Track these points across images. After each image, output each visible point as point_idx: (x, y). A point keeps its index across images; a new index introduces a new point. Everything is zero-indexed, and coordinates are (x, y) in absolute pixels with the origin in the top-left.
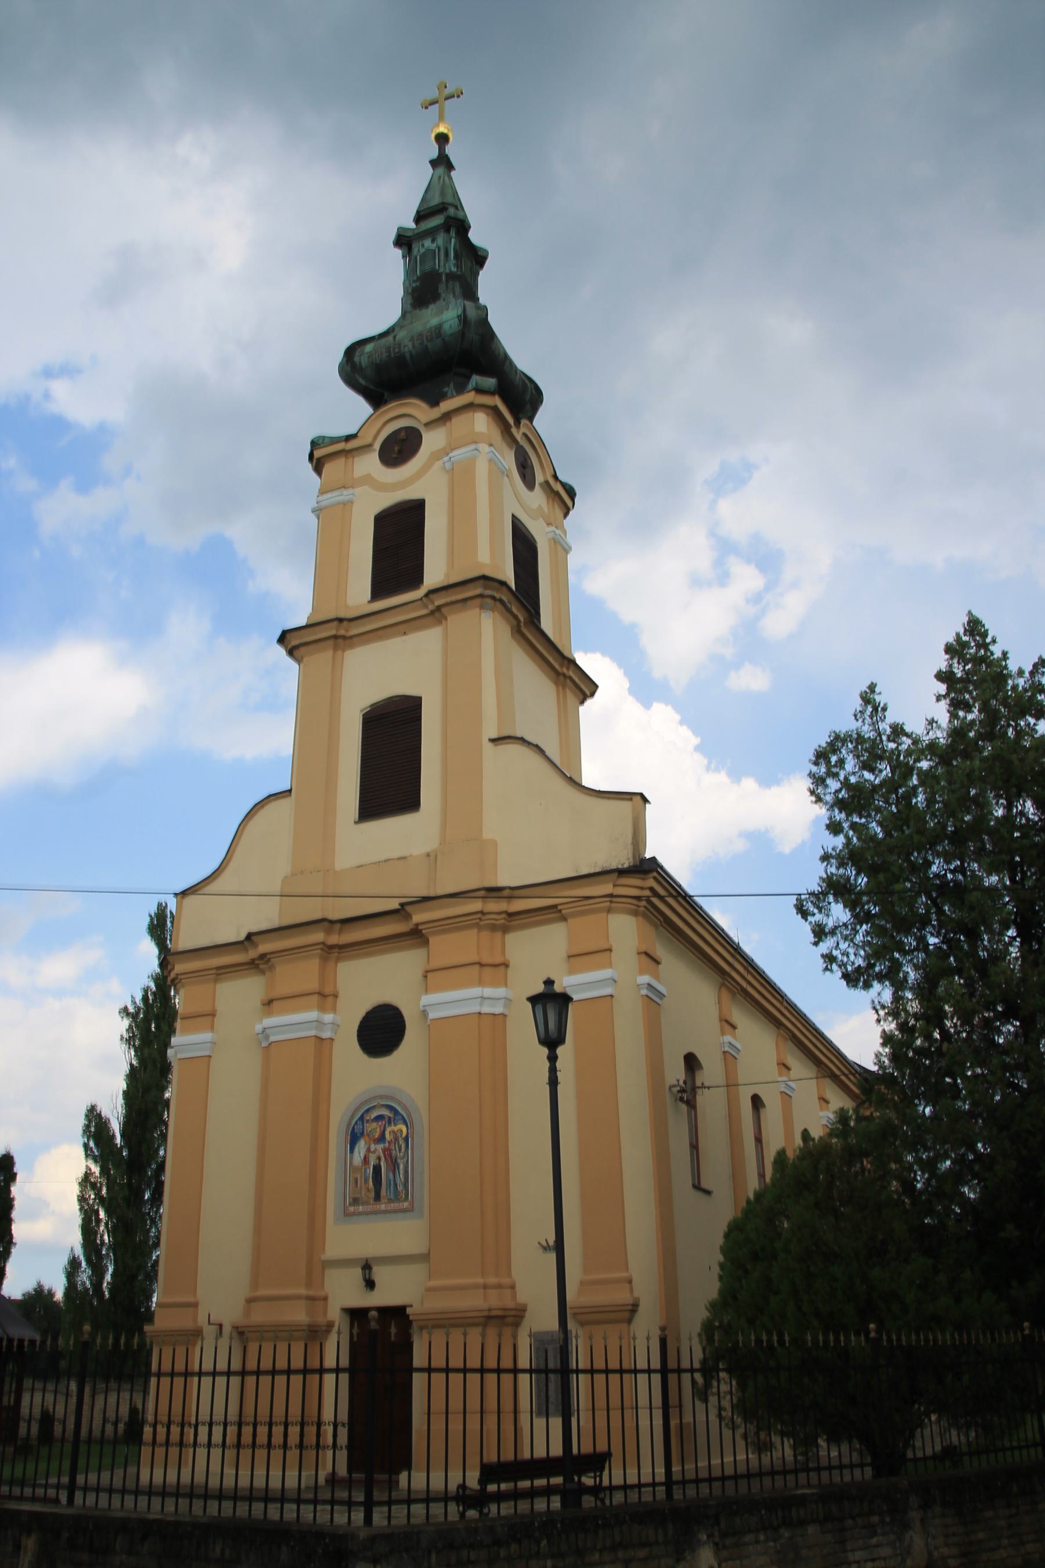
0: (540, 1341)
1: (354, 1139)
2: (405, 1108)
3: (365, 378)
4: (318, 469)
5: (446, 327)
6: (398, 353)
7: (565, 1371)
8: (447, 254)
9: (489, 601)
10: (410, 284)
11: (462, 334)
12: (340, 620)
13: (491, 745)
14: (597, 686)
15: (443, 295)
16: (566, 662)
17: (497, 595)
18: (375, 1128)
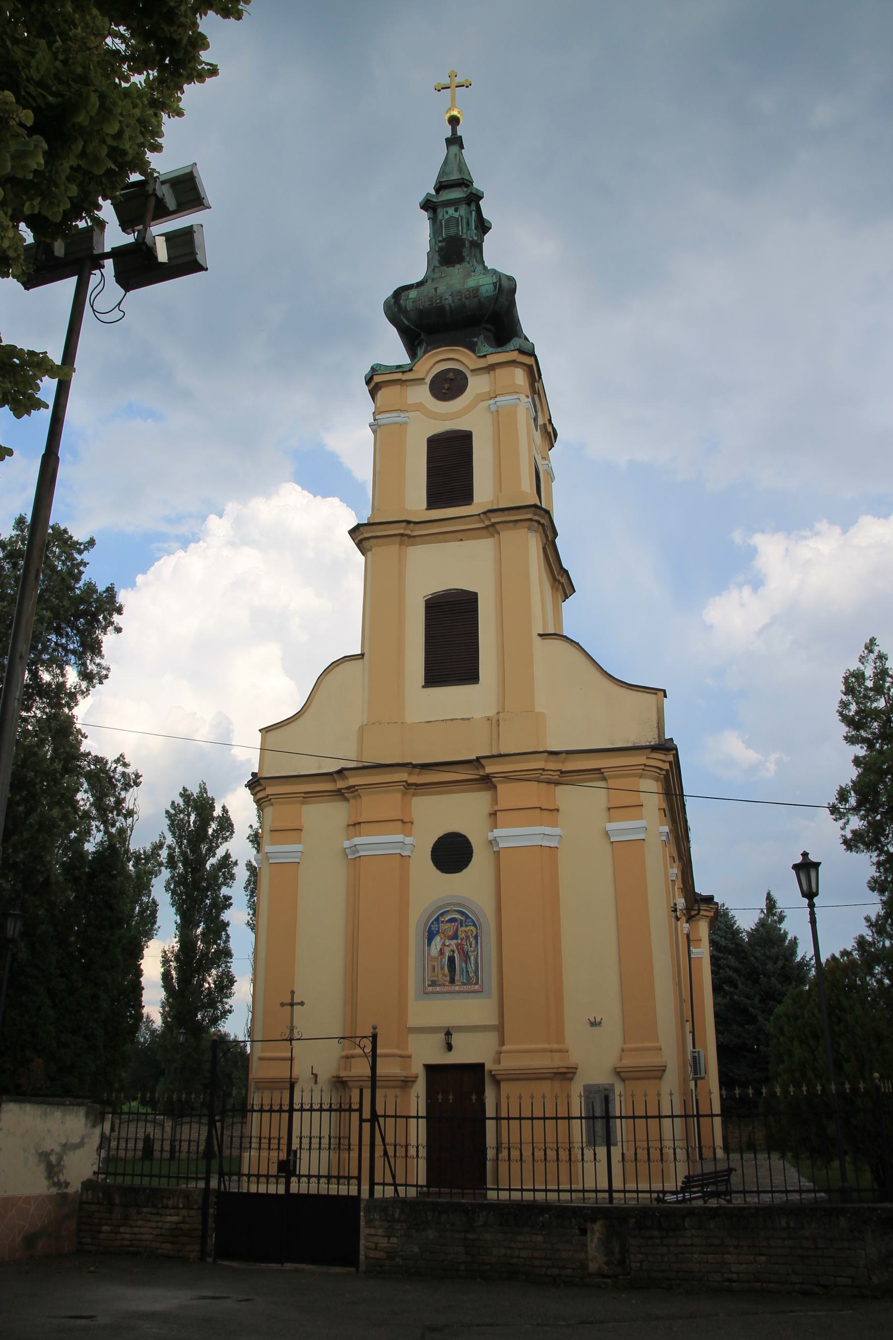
0: (590, 1092)
1: (431, 936)
2: (474, 913)
3: (408, 319)
4: (373, 393)
5: (483, 290)
6: (439, 303)
7: (608, 1117)
8: (468, 224)
9: (536, 524)
10: (436, 244)
11: (496, 298)
12: (409, 522)
13: (539, 638)
14: (575, 591)
15: (468, 259)
16: (562, 571)
17: (542, 521)
18: (449, 928)
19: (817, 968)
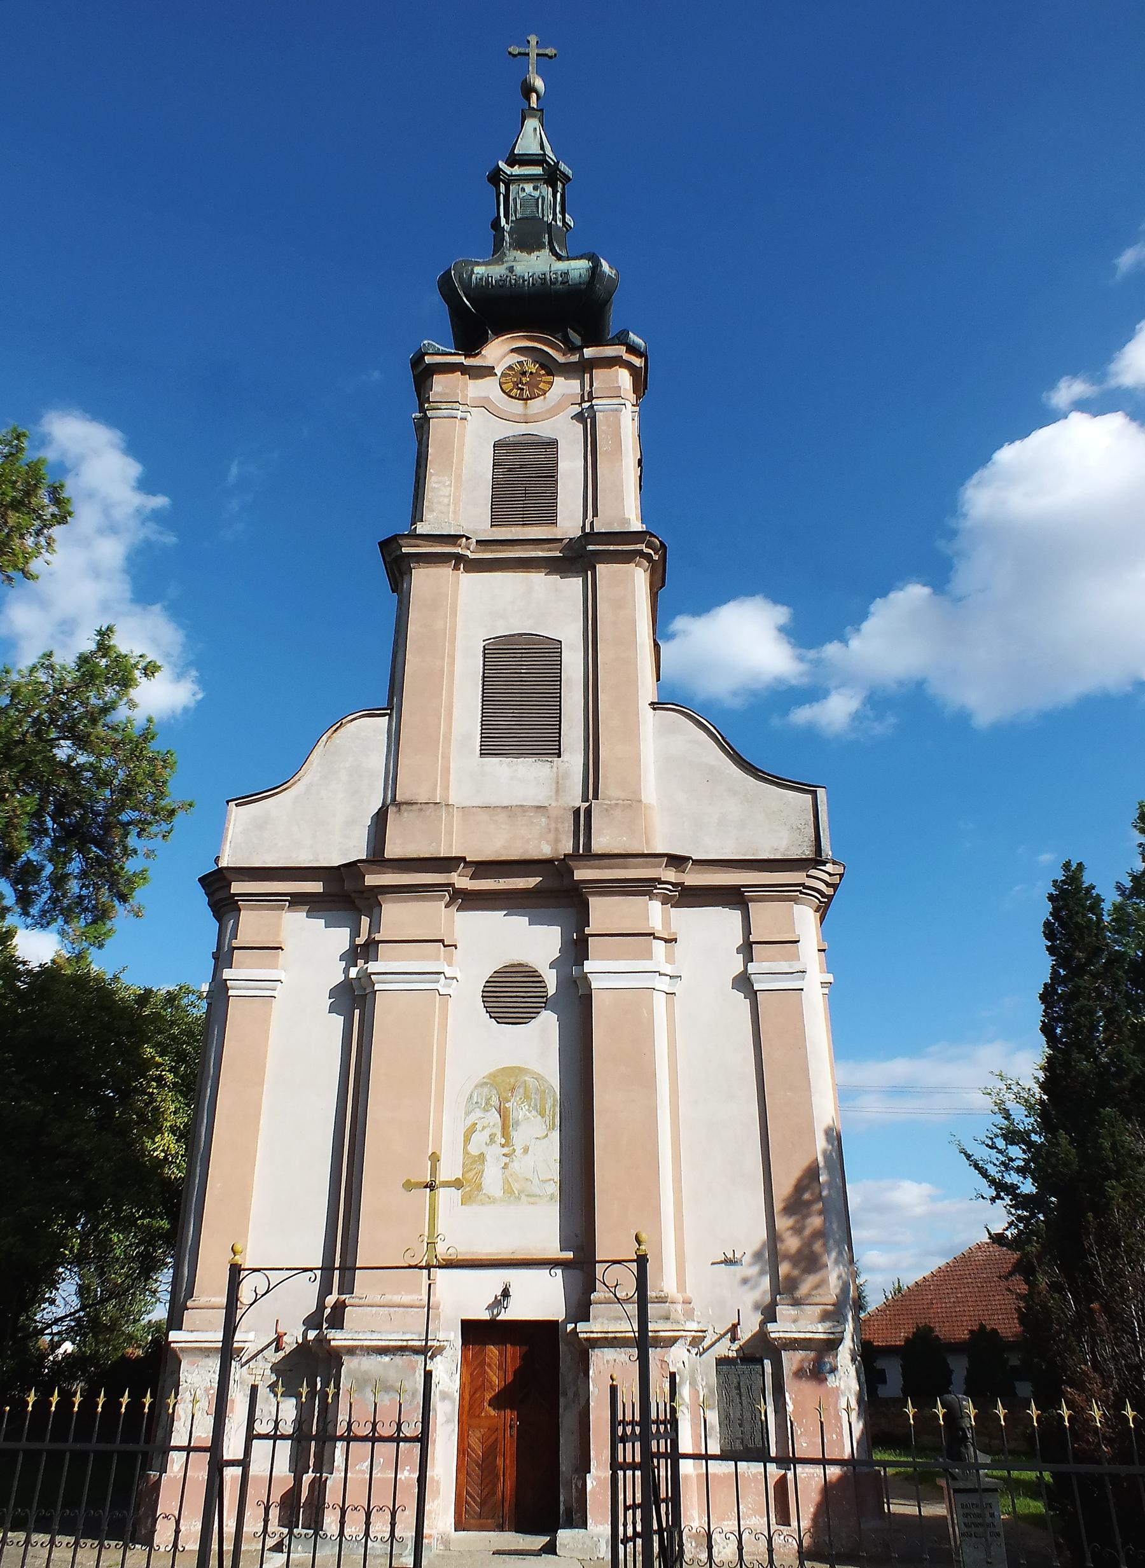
19: (1011, 1207)
